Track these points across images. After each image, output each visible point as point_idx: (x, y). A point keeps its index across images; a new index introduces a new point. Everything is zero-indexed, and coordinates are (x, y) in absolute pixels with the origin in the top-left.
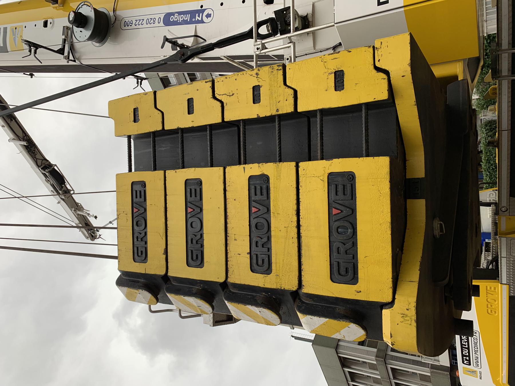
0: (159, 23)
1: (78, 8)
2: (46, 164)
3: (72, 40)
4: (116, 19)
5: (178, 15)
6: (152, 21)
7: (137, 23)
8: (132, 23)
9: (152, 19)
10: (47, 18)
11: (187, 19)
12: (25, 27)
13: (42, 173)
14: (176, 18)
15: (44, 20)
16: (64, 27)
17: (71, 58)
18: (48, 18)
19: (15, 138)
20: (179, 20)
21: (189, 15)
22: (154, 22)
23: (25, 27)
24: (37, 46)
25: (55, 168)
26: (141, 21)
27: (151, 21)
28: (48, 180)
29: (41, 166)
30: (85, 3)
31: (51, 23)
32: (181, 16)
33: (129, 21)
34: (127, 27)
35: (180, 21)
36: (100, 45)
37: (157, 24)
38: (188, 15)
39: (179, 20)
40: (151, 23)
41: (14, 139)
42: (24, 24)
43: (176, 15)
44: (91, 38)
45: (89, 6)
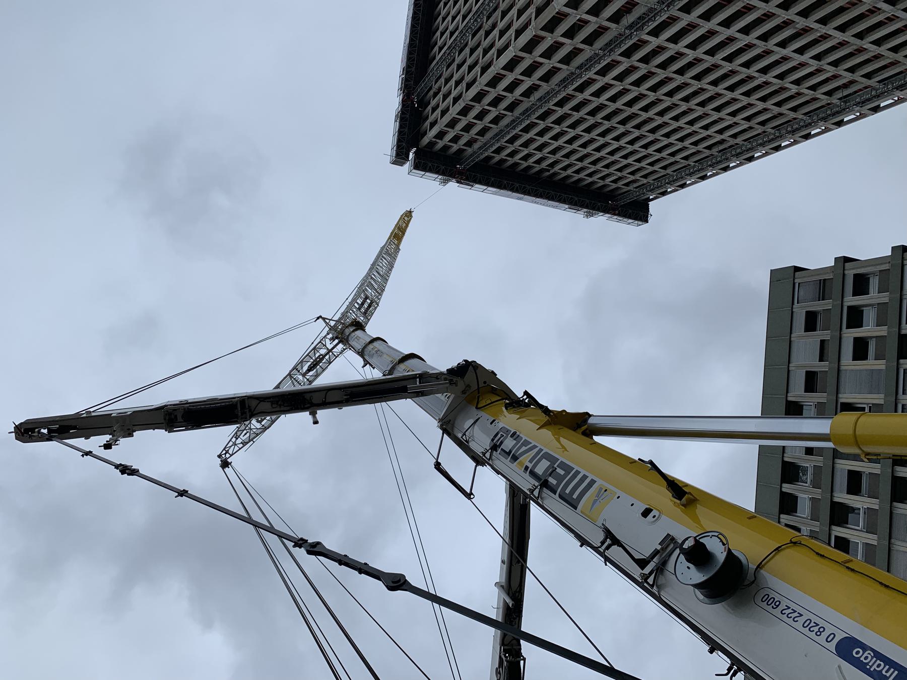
0: (827, 641)
1: (705, 534)
2: (515, 647)
3: (669, 558)
4: (753, 582)
5: (873, 655)
6: (816, 629)
7: (787, 612)
8: (778, 606)
9: (817, 625)
10: (653, 507)
11: (888, 675)
12: (618, 497)
13: (500, 657)
14: (866, 658)
15: (648, 507)
16: (668, 535)
17: (651, 580)
18: (655, 508)
19: (505, 587)
20: (870, 664)
21: (896, 672)
22: (818, 633)
23: (618, 497)
24: (616, 542)
25: (522, 662)
26: (796, 614)
27: (814, 627)
28: (500, 671)
29: (506, 645)
30: (720, 536)
31: (654, 517)
32: (878, 662)
33: (774, 599)
34: (764, 605)
35: (872, 669)
36: (708, 602)
37: (822, 639)
38: (893, 672)
39: (871, 667)
40: (812, 629)
41: (502, 586)
42: (619, 493)
43: (869, 654)
44: (697, 586)
45: (724, 544)
